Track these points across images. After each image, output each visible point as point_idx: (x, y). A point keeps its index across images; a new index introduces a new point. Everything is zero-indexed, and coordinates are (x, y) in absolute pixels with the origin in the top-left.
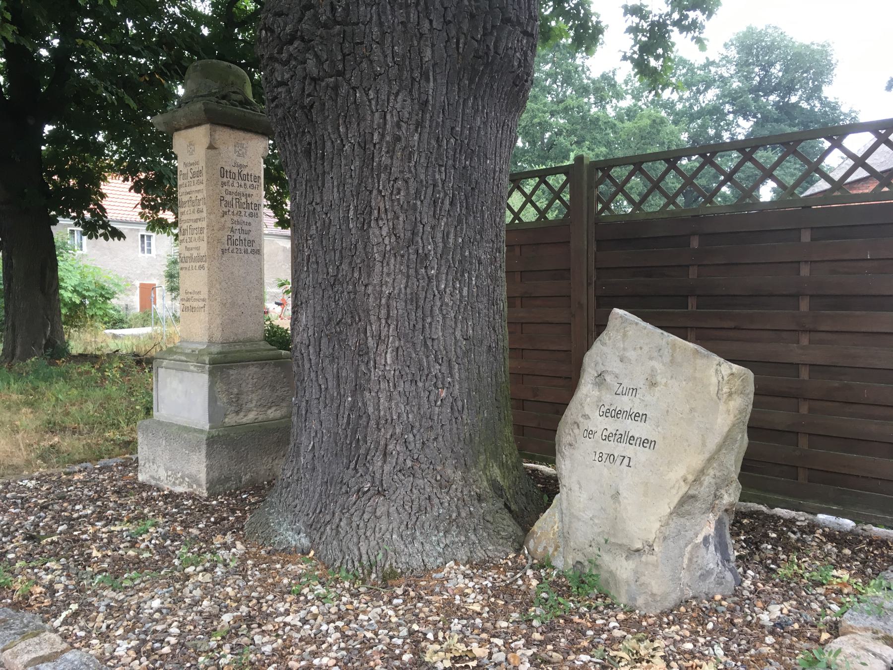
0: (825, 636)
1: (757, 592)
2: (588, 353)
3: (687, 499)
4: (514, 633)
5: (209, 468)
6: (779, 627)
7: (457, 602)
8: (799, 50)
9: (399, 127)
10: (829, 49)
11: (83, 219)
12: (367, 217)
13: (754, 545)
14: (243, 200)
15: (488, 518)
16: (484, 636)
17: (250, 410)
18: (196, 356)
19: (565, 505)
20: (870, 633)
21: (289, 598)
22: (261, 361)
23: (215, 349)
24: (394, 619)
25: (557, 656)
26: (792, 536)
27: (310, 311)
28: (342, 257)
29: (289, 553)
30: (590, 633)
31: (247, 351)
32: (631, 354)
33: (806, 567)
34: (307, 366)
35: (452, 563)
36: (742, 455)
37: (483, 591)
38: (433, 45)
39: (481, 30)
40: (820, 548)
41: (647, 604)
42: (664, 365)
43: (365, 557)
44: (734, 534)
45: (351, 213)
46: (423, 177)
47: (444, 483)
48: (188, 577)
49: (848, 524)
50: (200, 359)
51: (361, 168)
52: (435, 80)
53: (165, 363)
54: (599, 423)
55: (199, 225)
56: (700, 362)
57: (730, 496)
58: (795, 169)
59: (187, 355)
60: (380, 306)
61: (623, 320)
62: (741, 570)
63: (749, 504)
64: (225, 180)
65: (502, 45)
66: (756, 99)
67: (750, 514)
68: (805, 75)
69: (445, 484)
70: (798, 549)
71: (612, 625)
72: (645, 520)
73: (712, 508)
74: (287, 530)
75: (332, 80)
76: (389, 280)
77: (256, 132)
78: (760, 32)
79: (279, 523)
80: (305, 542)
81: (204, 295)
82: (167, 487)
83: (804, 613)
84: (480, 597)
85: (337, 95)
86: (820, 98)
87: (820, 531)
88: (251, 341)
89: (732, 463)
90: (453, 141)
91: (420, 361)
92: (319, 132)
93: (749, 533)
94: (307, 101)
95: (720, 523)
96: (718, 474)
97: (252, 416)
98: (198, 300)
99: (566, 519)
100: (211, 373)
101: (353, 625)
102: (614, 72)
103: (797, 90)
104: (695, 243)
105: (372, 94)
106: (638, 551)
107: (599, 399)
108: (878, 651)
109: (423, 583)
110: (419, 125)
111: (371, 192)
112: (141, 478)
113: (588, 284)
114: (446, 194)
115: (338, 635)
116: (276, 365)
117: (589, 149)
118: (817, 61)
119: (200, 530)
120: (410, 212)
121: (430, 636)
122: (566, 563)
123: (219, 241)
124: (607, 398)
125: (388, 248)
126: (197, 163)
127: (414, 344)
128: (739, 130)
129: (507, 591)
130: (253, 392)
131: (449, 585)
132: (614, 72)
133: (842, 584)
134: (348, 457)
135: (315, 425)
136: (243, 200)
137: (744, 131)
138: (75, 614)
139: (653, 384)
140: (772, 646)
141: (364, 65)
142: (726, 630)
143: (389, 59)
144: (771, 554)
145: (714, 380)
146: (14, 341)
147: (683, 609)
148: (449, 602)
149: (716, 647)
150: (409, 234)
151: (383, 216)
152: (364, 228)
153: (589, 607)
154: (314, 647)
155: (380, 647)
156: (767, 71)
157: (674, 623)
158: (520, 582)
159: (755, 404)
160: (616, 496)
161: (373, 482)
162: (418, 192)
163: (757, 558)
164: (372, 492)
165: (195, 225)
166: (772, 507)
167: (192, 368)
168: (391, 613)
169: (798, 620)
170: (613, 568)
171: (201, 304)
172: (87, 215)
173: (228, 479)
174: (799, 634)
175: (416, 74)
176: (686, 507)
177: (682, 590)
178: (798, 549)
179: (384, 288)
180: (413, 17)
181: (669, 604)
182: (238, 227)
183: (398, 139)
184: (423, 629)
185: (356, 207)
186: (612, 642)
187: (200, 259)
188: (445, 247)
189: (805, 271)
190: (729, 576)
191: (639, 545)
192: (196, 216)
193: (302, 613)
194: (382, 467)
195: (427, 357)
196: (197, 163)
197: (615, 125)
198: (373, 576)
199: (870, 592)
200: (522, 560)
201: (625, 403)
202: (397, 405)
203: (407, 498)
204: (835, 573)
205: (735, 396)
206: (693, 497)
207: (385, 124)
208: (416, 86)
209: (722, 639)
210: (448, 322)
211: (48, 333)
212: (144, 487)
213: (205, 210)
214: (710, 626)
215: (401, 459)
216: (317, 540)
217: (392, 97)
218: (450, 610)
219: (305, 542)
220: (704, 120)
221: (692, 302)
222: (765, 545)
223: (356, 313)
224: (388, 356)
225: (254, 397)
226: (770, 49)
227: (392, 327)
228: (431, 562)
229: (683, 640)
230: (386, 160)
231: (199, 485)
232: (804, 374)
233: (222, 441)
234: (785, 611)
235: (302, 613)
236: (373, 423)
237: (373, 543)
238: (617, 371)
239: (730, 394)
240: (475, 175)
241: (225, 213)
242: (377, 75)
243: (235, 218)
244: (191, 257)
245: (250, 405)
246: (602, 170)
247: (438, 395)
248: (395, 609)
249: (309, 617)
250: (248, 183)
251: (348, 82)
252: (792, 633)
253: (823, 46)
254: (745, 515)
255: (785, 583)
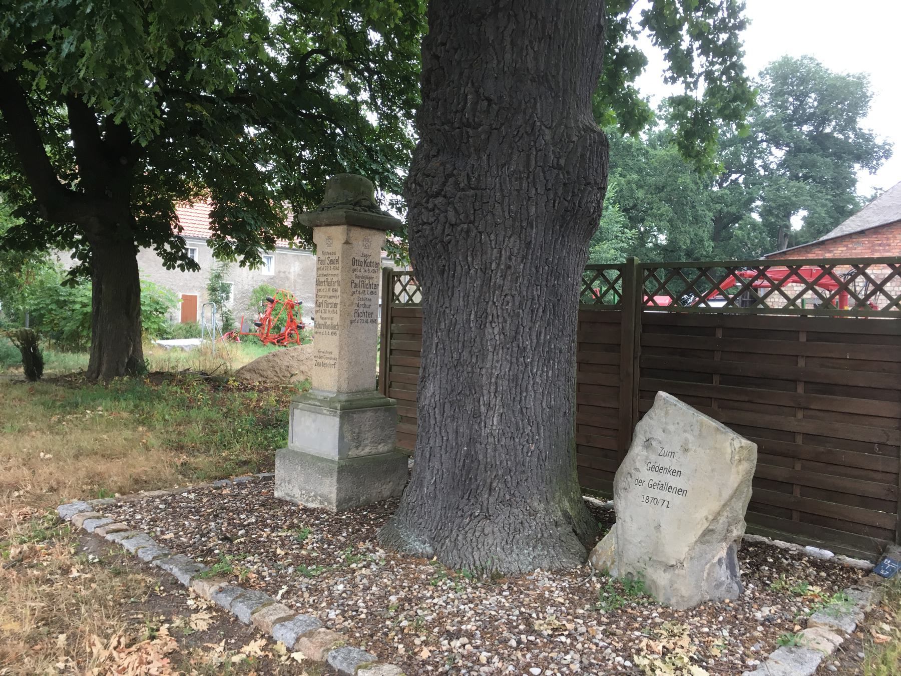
0: (797, 627)
1: (754, 599)
2: (639, 423)
3: (708, 532)
4: (589, 617)
5: (339, 490)
6: (768, 621)
7: (547, 596)
8: (834, 82)
9: (510, 259)
10: (865, 81)
11: (165, 251)
12: (484, 320)
13: (756, 566)
14: (367, 282)
15: (562, 539)
16: (570, 617)
17: (366, 446)
18: (328, 403)
19: (620, 532)
20: (827, 627)
21: (431, 588)
22: (376, 407)
23: (343, 398)
24: (507, 605)
25: (619, 632)
26: (785, 561)
27: (437, 383)
28: (463, 346)
29: (419, 558)
30: (640, 619)
31: (368, 399)
32: (671, 428)
33: (792, 583)
34: (432, 422)
35: (539, 570)
36: (748, 501)
37: (563, 589)
38: (537, 204)
39: (570, 194)
40: (804, 570)
41: (678, 603)
42: (694, 436)
43: (478, 563)
44: (740, 558)
45: (472, 317)
46: (525, 293)
47: (532, 512)
48: (354, 571)
49: (828, 554)
50: (333, 405)
51: (482, 286)
52: (537, 227)
53: (301, 405)
54: (646, 475)
55: (333, 300)
56: (720, 437)
57: (738, 531)
58: (827, 199)
59: (319, 400)
60: (490, 383)
61: (666, 401)
62: (744, 583)
63: (755, 536)
64: (355, 267)
65: (584, 201)
66: (789, 128)
67: (755, 544)
68: (840, 106)
69: (533, 513)
70: (787, 571)
71: (654, 615)
72: (679, 545)
73: (725, 539)
74: (415, 541)
75: (466, 226)
76: (497, 366)
77: (378, 229)
78: (795, 63)
79: (407, 535)
80: (429, 550)
81: (336, 354)
82: (302, 503)
83: (785, 613)
84: (562, 593)
85: (468, 236)
86: (854, 129)
87: (807, 559)
88: (367, 390)
89: (740, 508)
90: (546, 268)
91: (517, 423)
92: (453, 260)
93: (752, 557)
94: (446, 239)
95: (730, 549)
96: (730, 515)
97: (367, 450)
98: (330, 359)
99: (621, 542)
100: (341, 417)
101: (480, 607)
102: (647, 99)
103: (830, 121)
104: (719, 334)
105: (493, 237)
106: (672, 566)
107: (647, 458)
108: (831, 638)
109: (520, 582)
110: (524, 257)
111: (487, 303)
112: (277, 494)
113: (635, 358)
114: (540, 305)
115: (473, 612)
116: (386, 410)
117: (621, 175)
118: (852, 93)
119: (344, 537)
120: (515, 318)
121: (534, 615)
122: (620, 574)
123: (349, 314)
124: (653, 457)
125: (498, 343)
126: (334, 253)
127: (513, 411)
128: (771, 158)
129: (579, 590)
130: (369, 431)
131: (539, 584)
132: (647, 99)
133: (815, 595)
134: (463, 490)
135: (437, 465)
136: (367, 282)
137: (776, 160)
138: (288, 592)
139: (686, 450)
140: (762, 632)
141: (489, 217)
142: (732, 622)
143: (506, 214)
144: (767, 573)
145: (729, 450)
146: (100, 358)
147: (702, 607)
148: (541, 596)
149: (724, 631)
150: (513, 333)
151: (496, 320)
152: (481, 327)
153: (638, 603)
154: (459, 619)
155: (503, 620)
156: (801, 102)
157: (696, 616)
158: (588, 585)
159: (759, 460)
160: (658, 527)
161: (481, 509)
162: (521, 304)
163: (757, 575)
164: (481, 516)
165: (330, 301)
166: (773, 540)
167: (325, 412)
168: (503, 600)
169: (781, 618)
170: (654, 577)
171: (332, 362)
172: (167, 247)
173: (350, 499)
174: (780, 626)
175: (524, 224)
176: (707, 538)
177: (702, 595)
178: (787, 571)
179: (494, 371)
180: (525, 185)
181: (693, 603)
182: (362, 303)
183: (509, 267)
184: (528, 611)
185: (476, 313)
186: (655, 625)
187: (333, 327)
188: (538, 342)
189: (801, 363)
190: (735, 587)
191: (674, 563)
192: (331, 294)
193: (444, 598)
194: (488, 499)
195: (522, 420)
196: (334, 253)
197: (647, 152)
198: (485, 576)
199: (833, 601)
200: (587, 570)
201: (665, 462)
202: (500, 454)
203: (506, 522)
204: (810, 587)
205: (743, 462)
206: (712, 530)
207: (501, 256)
208: (524, 231)
209: (729, 626)
210: (537, 396)
211: (131, 352)
212: (281, 502)
213: (339, 290)
214: (721, 619)
215: (502, 494)
216: (439, 549)
217: (507, 239)
218: (543, 601)
219: (429, 550)
220: (736, 148)
221: (716, 379)
222: (763, 567)
223: (473, 387)
224: (495, 419)
225: (369, 435)
226: (803, 80)
227: (499, 398)
228: (525, 568)
229: (702, 626)
230: (499, 281)
231: (330, 503)
232: (799, 440)
233: (350, 470)
234: (773, 611)
235: (444, 598)
236: (482, 467)
237: (483, 553)
238: (661, 439)
239: (740, 461)
240: (561, 290)
241: (354, 293)
242: (496, 224)
243: (361, 296)
244: (325, 326)
245: (366, 442)
246: (649, 270)
247: (529, 448)
248: (506, 597)
249: (449, 600)
250: (371, 269)
251: (477, 228)
252: (775, 625)
253: (859, 78)
254: (751, 544)
255: (775, 593)
